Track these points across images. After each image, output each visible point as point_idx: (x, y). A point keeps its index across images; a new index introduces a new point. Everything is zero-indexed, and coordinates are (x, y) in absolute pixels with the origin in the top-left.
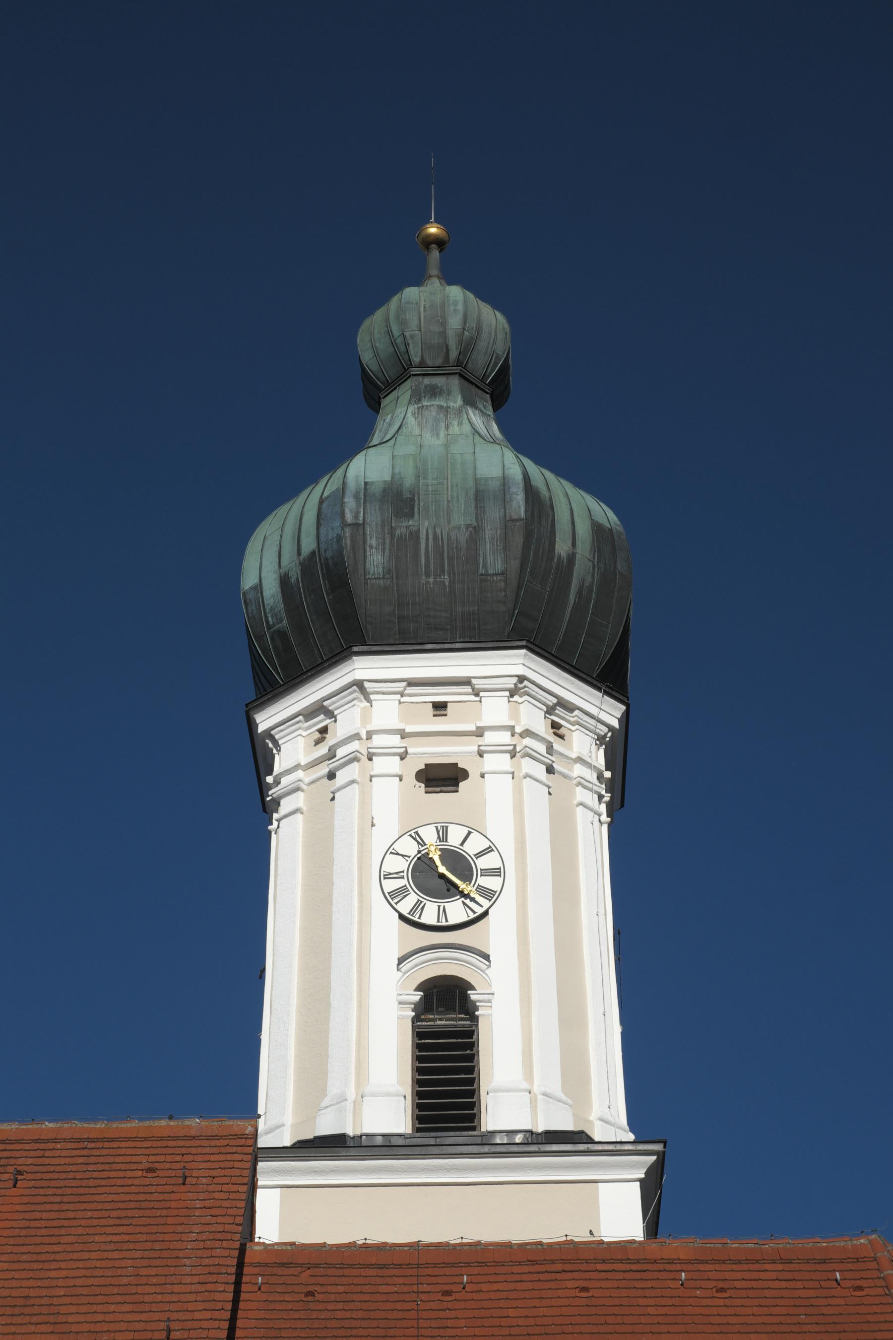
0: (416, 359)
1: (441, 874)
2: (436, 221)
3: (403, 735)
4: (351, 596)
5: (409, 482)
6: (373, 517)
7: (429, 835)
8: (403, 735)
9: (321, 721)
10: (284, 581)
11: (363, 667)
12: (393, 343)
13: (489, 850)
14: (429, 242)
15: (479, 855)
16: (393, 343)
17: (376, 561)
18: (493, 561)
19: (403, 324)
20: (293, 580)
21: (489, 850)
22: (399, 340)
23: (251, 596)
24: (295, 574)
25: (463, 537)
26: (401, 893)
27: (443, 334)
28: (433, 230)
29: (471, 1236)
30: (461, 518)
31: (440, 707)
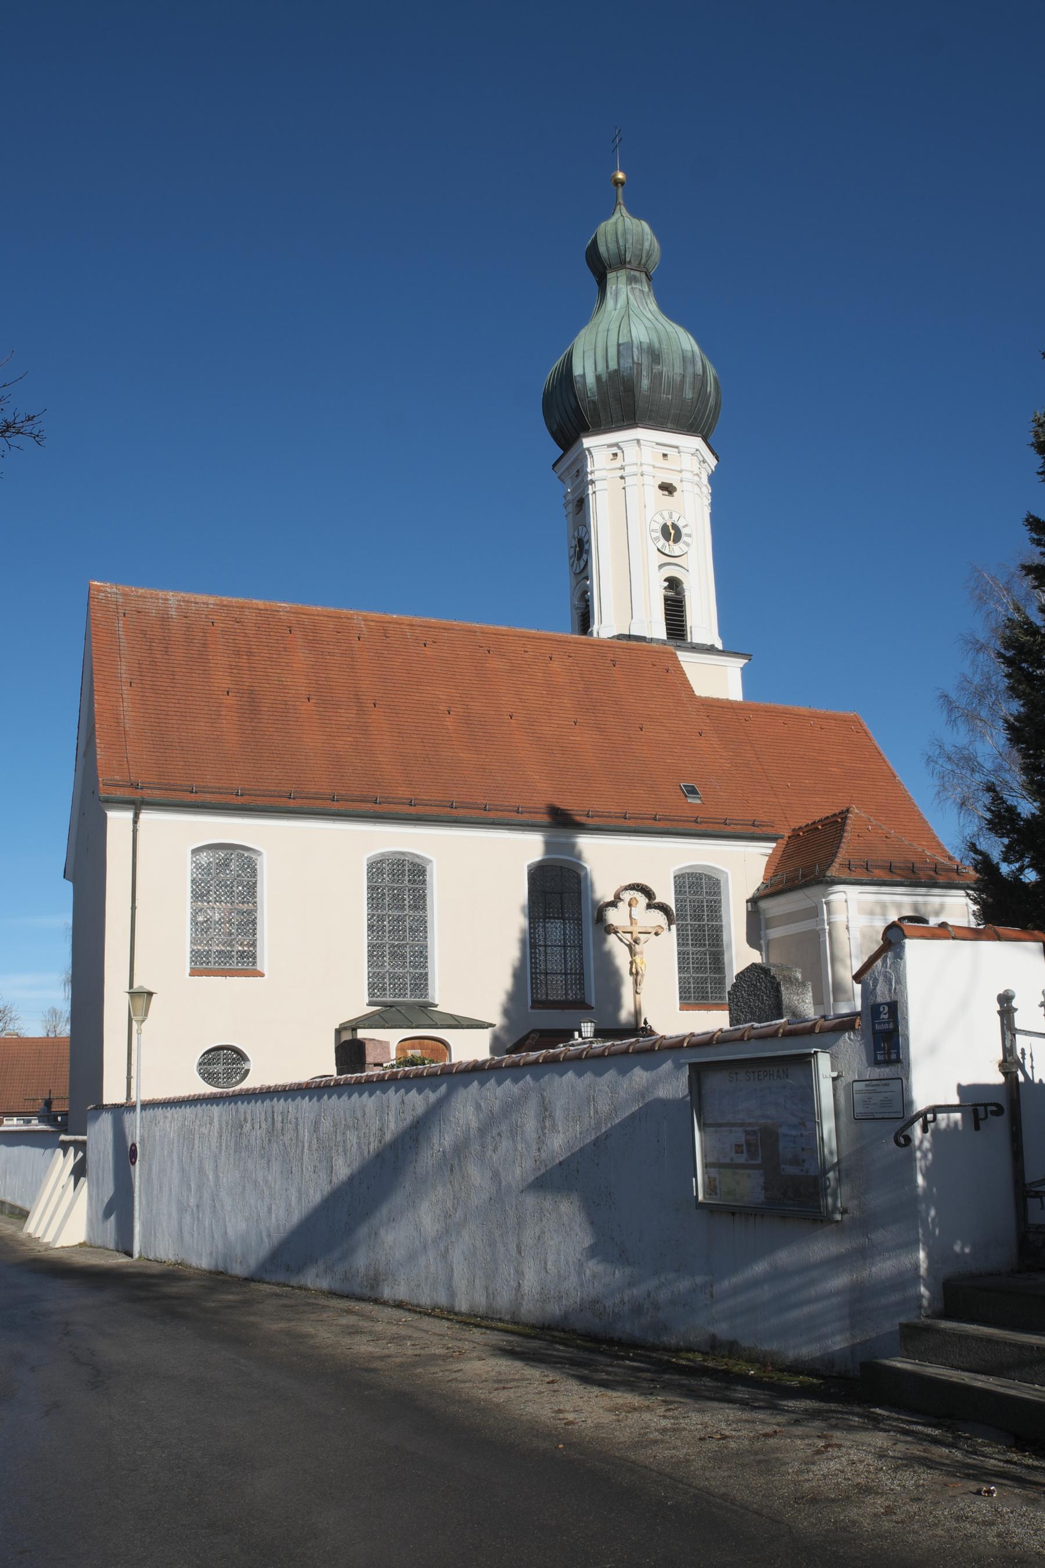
0: (628, 259)
1: (671, 533)
2: (621, 171)
3: (654, 467)
4: (634, 396)
5: (657, 345)
6: (645, 361)
7: (667, 517)
8: (654, 467)
9: (615, 450)
10: (598, 378)
11: (639, 433)
12: (618, 248)
13: (661, 515)
14: (617, 183)
15: (684, 527)
16: (618, 248)
17: (645, 383)
18: (689, 394)
19: (626, 241)
20: (604, 380)
21: (661, 515)
22: (622, 248)
23: (578, 379)
24: (604, 378)
25: (678, 379)
26: (657, 539)
27: (642, 250)
28: (620, 176)
29: (715, 696)
30: (678, 370)
31: (665, 455)
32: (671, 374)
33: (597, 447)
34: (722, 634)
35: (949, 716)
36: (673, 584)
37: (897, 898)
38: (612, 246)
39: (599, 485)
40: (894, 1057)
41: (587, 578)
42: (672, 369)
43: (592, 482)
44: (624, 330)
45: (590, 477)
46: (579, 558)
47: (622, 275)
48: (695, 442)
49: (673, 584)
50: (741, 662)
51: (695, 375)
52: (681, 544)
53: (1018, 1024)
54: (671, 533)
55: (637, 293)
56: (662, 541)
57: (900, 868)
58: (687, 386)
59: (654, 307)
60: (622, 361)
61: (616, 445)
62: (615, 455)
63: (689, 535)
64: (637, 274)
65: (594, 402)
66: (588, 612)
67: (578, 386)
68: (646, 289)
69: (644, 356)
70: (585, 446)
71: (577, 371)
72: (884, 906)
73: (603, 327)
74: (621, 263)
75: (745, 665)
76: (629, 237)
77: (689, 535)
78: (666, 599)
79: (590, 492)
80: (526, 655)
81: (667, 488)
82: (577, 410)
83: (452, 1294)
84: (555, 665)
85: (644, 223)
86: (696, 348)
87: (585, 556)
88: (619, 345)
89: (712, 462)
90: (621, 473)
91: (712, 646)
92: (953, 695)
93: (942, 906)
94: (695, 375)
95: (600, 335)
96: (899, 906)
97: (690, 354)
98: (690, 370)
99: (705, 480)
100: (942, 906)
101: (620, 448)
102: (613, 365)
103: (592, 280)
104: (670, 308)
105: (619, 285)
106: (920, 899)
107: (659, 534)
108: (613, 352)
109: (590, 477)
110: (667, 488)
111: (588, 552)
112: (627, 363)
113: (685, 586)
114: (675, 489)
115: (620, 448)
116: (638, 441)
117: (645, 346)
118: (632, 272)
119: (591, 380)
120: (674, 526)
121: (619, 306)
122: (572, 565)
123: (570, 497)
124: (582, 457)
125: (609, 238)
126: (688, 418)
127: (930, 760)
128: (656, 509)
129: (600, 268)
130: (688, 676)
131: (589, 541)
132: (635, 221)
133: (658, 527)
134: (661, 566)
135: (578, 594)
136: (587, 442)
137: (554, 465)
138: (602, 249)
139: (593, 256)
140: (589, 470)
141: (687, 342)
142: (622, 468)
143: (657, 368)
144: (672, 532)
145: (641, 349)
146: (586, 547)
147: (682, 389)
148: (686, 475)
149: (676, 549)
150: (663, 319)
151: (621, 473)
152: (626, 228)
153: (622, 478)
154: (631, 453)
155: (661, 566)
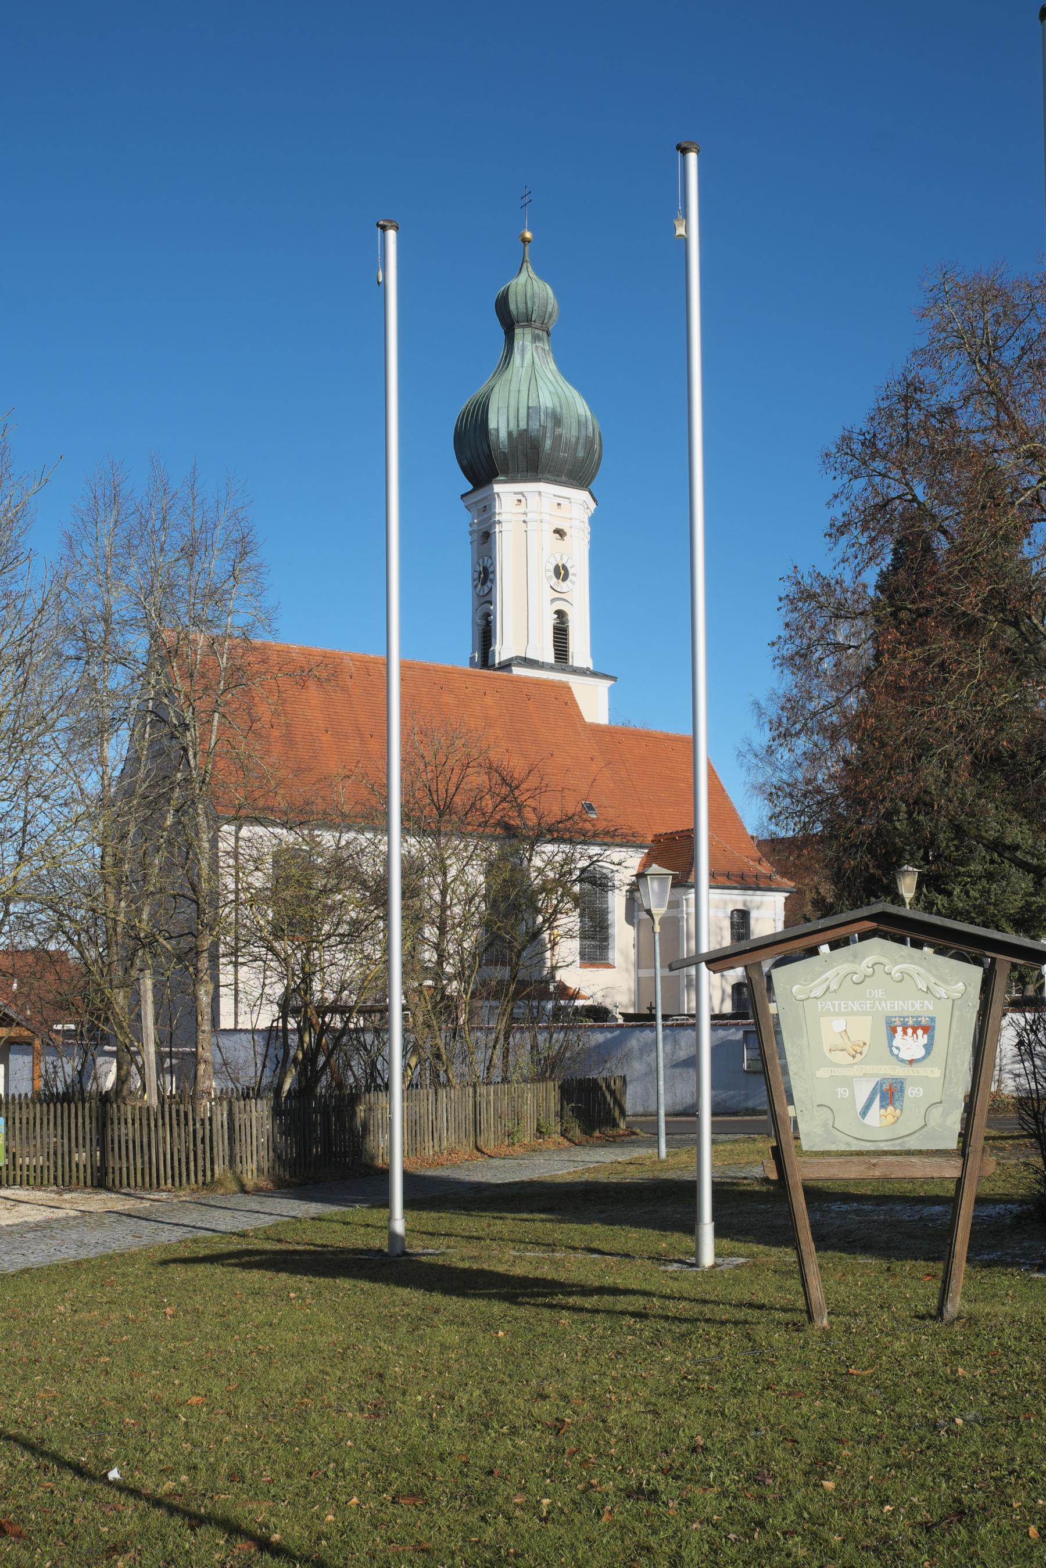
1: (561, 572)
5: (558, 410)
6: (549, 424)
9: (520, 497)
14: (525, 241)
17: (548, 443)
18: (581, 453)
19: (534, 303)
22: (530, 309)
23: (493, 432)
25: (574, 440)
26: (551, 577)
28: (528, 235)
30: (574, 433)
31: (559, 504)
32: (568, 436)
33: (506, 494)
34: (593, 655)
35: (758, 720)
36: (561, 614)
37: (734, 897)
38: (522, 306)
39: (505, 526)
41: (490, 603)
42: (570, 432)
43: (500, 522)
44: (533, 395)
45: (497, 518)
46: (483, 584)
47: (528, 332)
48: (583, 495)
49: (561, 614)
50: (609, 683)
51: (587, 437)
53: (232, 1027)
54: (561, 572)
55: (540, 351)
56: (554, 579)
57: (736, 876)
59: (553, 366)
60: (530, 423)
61: (522, 493)
62: (520, 501)
63: (574, 575)
64: (540, 332)
65: (504, 453)
66: (490, 631)
67: (492, 438)
68: (547, 348)
69: (549, 420)
70: (495, 491)
71: (492, 424)
72: (725, 903)
73: (514, 387)
74: (528, 320)
75: (612, 686)
76: (536, 301)
77: (574, 575)
78: (555, 628)
79: (497, 530)
80: (467, 691)
81: (560, 533)
82: (489, 457)
84: (489, 700)
85: (548, 286)
86: (589, 413)
87: (489, 584)
88: (528, 408)
89: (593, 506)
90: (524, 517)
91: (588, 669)
92: (763, 703)
93: (762, 903)
94: (587, 437)
96: (735, 902)
97: (583, 419)
98: (583, 433)
99: (586, 521)
100: (762, 903)
101: (524, 496)
102: (523, 425)
103: (501, 332)
104: (568, 370)
105: (523, 338)
106: (748, 898)
107: (552, 573)
108: (523, 413)
109: (497, 518)
110: (560, 533)
111: (493, 581)
112: (535, 425)
113: (570, 618)
114: (565, 534)
115: (524, 496)
116: (540, 493)
117: (549, 411)
118: (537, 331)
119: (503, 434)
120: (564, 567)
121: (525, 364)
122: (476, 587)
123: (475, 527)
124: (492, 498)
125: (519, 298)
126: (578, 473)
127: (740, 754)
128: (548, 552)
129: (509, 321)
130: (581, 708)
131: (494, 572)
132: (541, 283)
133: (552, 568)
135: (480, 613)
136: (497, 488)
137: (463, 496)
138: (512, 307)
139: (502, 305)
140: (497, 511)
141: (581, 407)
142: (525, 514)
143: (558, 431)
144: (563, 572)
145: (546, 415)
146: (491, 576)
147: (576, 450)
149: (563, 586)
150: (561, 379)
151: (524, 517)
152: (530, 287)
153: (525, 522)
154: (532, 501)
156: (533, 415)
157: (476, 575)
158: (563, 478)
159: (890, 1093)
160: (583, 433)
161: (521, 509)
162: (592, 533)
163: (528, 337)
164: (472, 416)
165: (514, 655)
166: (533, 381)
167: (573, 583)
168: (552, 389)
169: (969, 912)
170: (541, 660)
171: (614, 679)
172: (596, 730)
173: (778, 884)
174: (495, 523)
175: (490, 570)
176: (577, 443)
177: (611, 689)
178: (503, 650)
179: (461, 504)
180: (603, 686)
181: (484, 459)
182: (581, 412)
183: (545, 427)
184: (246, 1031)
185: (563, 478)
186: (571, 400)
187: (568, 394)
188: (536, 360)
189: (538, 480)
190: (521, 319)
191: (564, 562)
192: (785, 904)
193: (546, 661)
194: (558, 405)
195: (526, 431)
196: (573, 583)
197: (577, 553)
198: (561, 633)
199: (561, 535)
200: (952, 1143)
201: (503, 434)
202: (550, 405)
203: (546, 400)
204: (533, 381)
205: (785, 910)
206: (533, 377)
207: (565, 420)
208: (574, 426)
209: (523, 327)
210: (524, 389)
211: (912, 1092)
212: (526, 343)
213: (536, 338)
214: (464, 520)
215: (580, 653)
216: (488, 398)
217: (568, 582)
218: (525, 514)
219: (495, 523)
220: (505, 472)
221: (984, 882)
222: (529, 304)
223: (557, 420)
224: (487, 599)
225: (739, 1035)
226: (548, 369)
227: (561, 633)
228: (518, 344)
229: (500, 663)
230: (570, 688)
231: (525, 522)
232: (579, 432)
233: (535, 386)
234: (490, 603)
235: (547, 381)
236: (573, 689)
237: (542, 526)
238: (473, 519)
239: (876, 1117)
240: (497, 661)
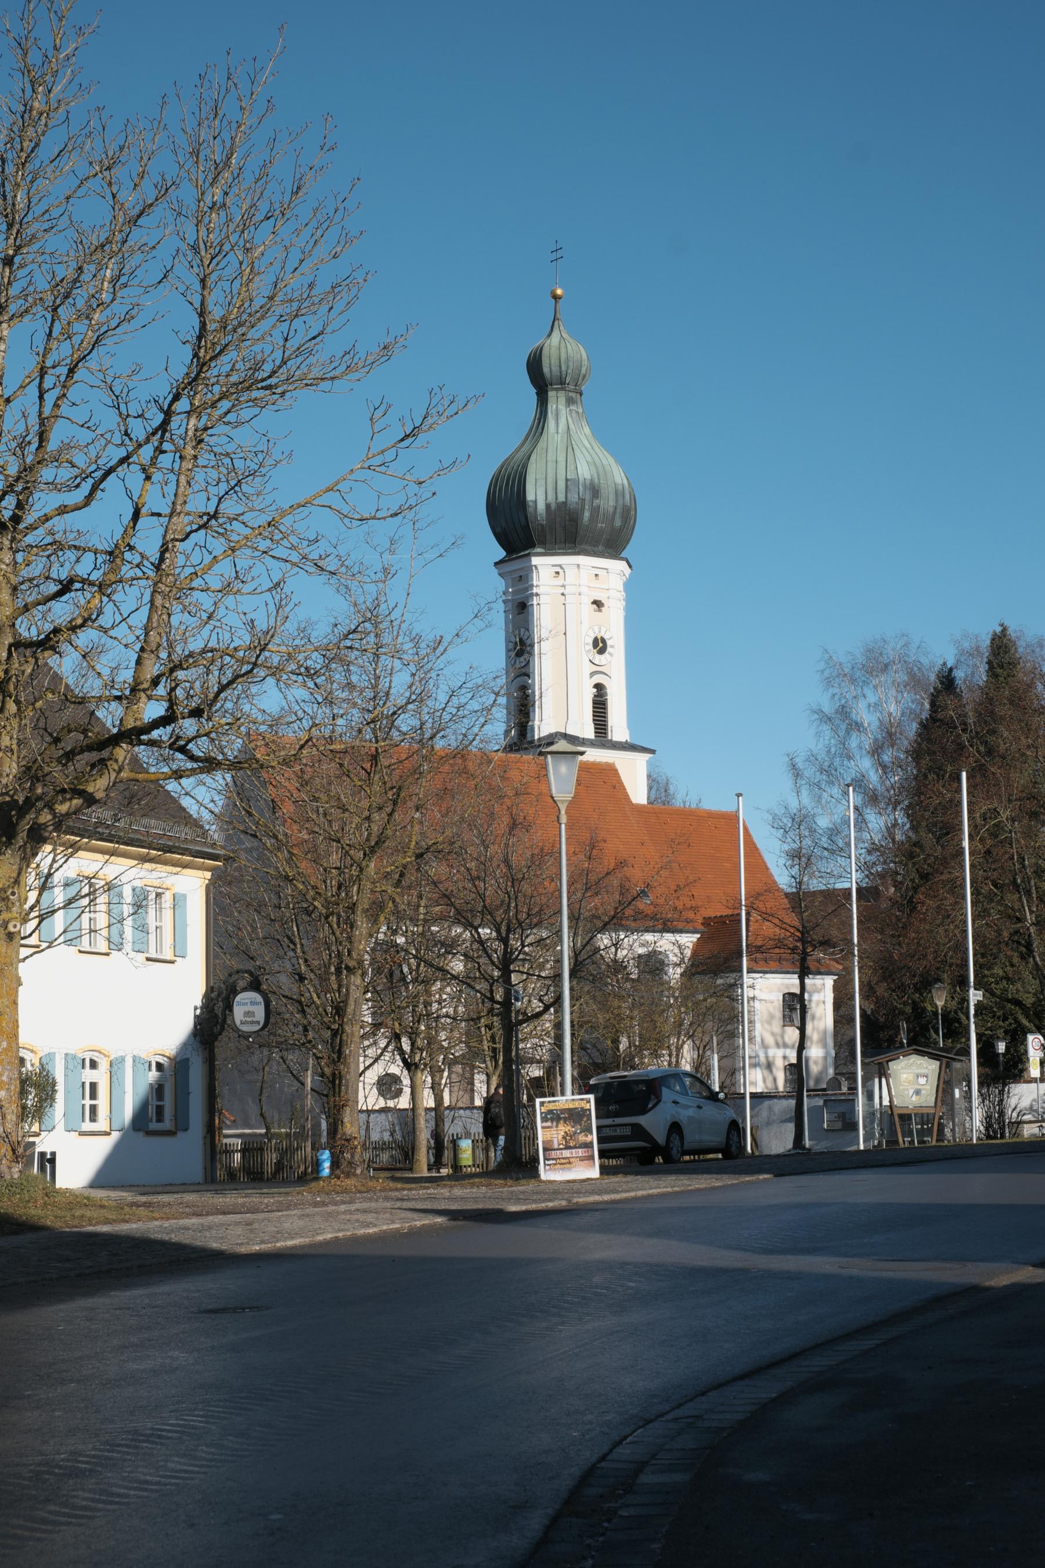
1: (600, 645)
5: (596, 481)
6: (588, 497)
9: (558, 569)
10: (548, 506)
14: (556, 297)
17: (587, 514)
18: (618, 523)
19: (568, 367)
22: (564, 373)
23: (531, 504)
25: (611, 510)
26: (589, 651)
28: (559, 292)
30: (612, 503)
31: (596, 575)
33: (544, 568)
34: (630, 726)
39: (543, 599)
40: (408, 1166)
43: (537, 595)
44: (571, 467)
45: (535, 590)
47: (562, 394)
48: (621, 565)
49: (599, 687)
50: (647, 756)
51: (624, 506)
52: (602, 657)
54: (600, 645)
55: (574, 415)
58: (618, 516)
61: (560, 566)
62: (558, 573)
63: (612, 647)
64: (573, 395)
65: (542, 525)
67: (530, 510)
70: (533, 563)
71: (530, 496)
73: (551, 456)
76: (571, 364)
77: (612, 647)
78: (595, 702)
79: (535, 602)
81: (598, 604)
82: (526, 527)
83: (776, 1088)
87: (526, 656)
88: (567, 480)
89: (627, 571)
90: (562, 590)
94: (624, 506)
95: (551, 466)
97: (620, 488)
99: (621, 588)
101: (562, 568)
102: (561, 498)
105: (557, 401)
108: (562, 485)
109: (535, 590)
110: (598, 604)
111: (531, 654)
112: (573, 498)
113: (609, 691)
115: (562, 568)
117: (588, 482)
118: (570, 394)
119: (541, 506)
120: (603, 641)
121: (560, 430)
124: (530, 569)
128: (586, 625)
130: (629, 791)
134: (592, 674)
136: (535, 560)
137: (496, 564)
138: (546, 370)
142: (564, 586)
143: (596, 502)
144: (601, 645)
145: (585, 486)
147: (613, 519)
148: (612, 593)
151: (562, 590)
153: (563, 594)
154: (571, 572)
155: (592, 674)
156: (571, 487)
157: (511, 646)
158: (601, 548)
159: (918, 1092)
160: (620, 502)
161: (560, 581)
162: (628, 600)
163: (562, 400)
164: (508, 480)
165: (553, 731)
166: (570, 450)
167: (611, 655)
168: (589, 459)
169: (992, 1007)
170: (581, 736)
171: (653, 752)
172: (638, 808)
173: (828, 966)
174: (532, 595)
175: (528, 642)
176: (614, 513)
177: (648, 762)
178: (544, 724)
179: (495, 571)
180: (641, 760)
181: (520, 529)
182: (618, 480)
183: (584, 500)
184: (363, 1111)
185: (601, 548)
186: (608, 468)
187: (605, 462)
188: (572, 426)
189: (578, 553)
190: (554, 381)
191: (602, 634)
192: (834, 986)
193: (586, 737)
194: (595, 475)
195: (565, 503)
196: (611, 655)
197: (613, 625)
198: (600, 705)
199: (598, 606)
200: (933, 1104)
201: (541, 506)
202: (588, 476)
203: (585, 472)
204: (570, 450)
205: (834, 992)
206: (570, 447)
207: (603, 491)
208: (612, 497)
209: (557, 390)
210: (561, 458)
211: (923, 1092)
212: (560, 407)
213: (570, 401)
214: (494, 586)
215: (619, 729)
216: (525, 467)
217: (606, 655)
218: (564, 586)
219: (532, 595)
220: (543, 543)
221: (1005, 982)
222: (564, 368)
223: (595, 491)
224: (523, 670)
225: (821, 1103)
226: (583, 435)
227: (600, 705)
228: (551, 407)
229: (539, 739)
230: (616, 770)
231: (563, 594)
232: (617, 501)
233: (573, 457)
234: (529, 676)
235: (584, 450)
236: (620, 772)
237: (577, 595)
238: (507, 588)
239: (914, 1098)
240: (536, 737)
